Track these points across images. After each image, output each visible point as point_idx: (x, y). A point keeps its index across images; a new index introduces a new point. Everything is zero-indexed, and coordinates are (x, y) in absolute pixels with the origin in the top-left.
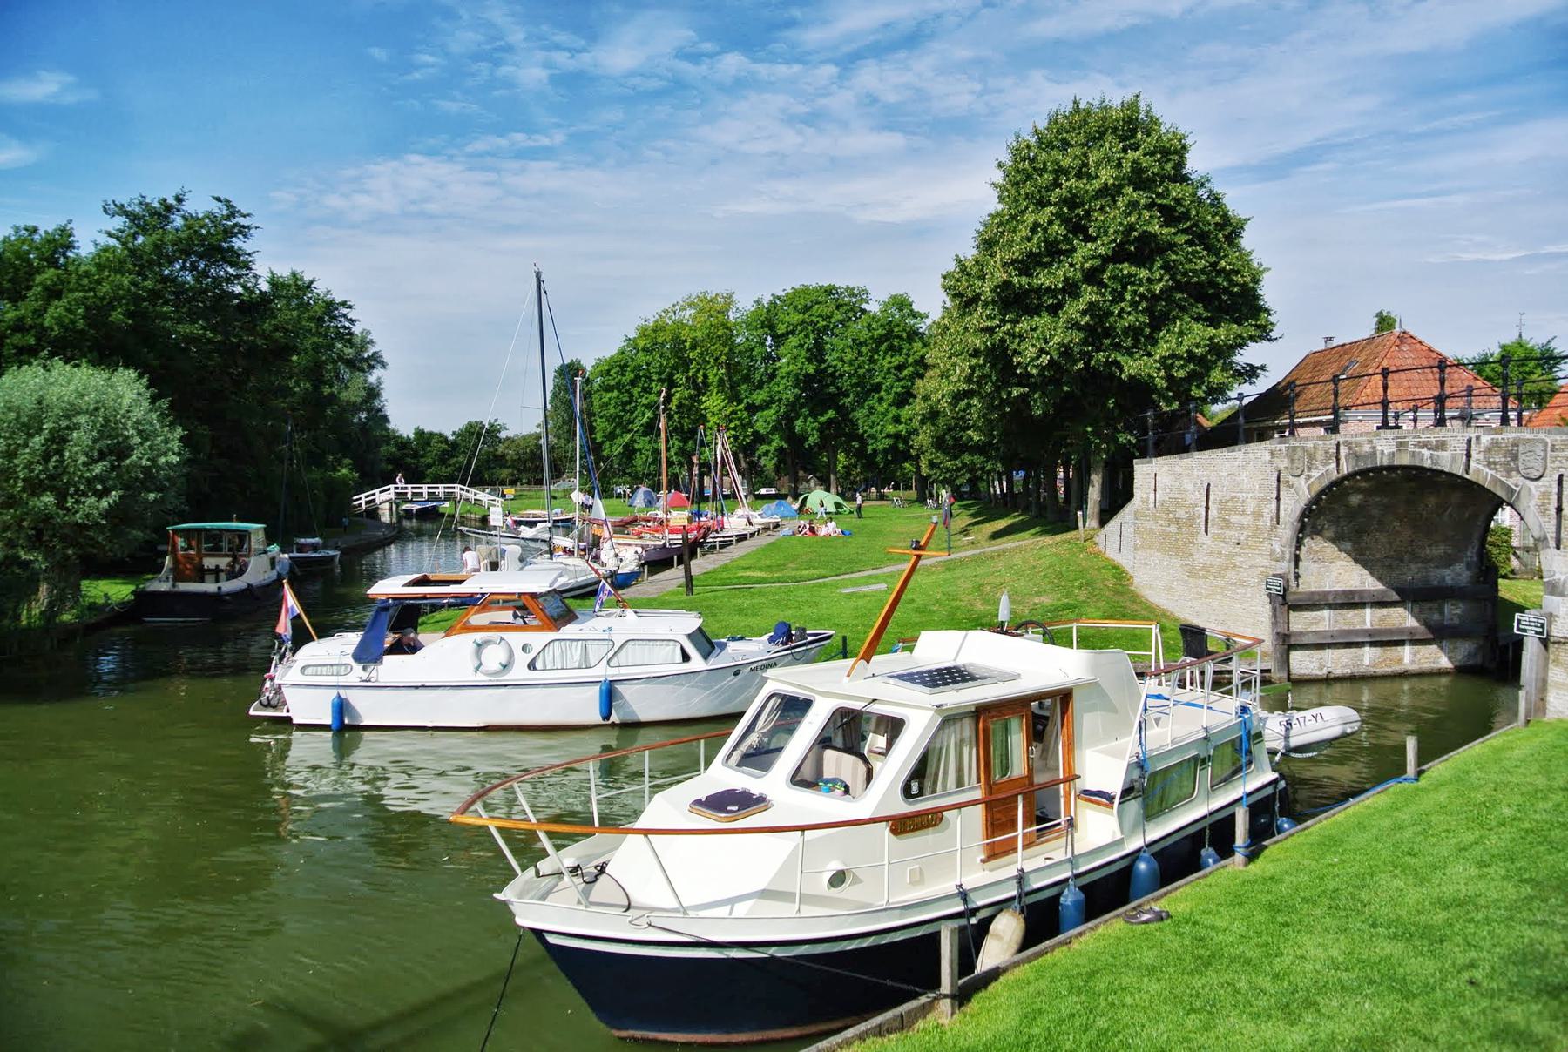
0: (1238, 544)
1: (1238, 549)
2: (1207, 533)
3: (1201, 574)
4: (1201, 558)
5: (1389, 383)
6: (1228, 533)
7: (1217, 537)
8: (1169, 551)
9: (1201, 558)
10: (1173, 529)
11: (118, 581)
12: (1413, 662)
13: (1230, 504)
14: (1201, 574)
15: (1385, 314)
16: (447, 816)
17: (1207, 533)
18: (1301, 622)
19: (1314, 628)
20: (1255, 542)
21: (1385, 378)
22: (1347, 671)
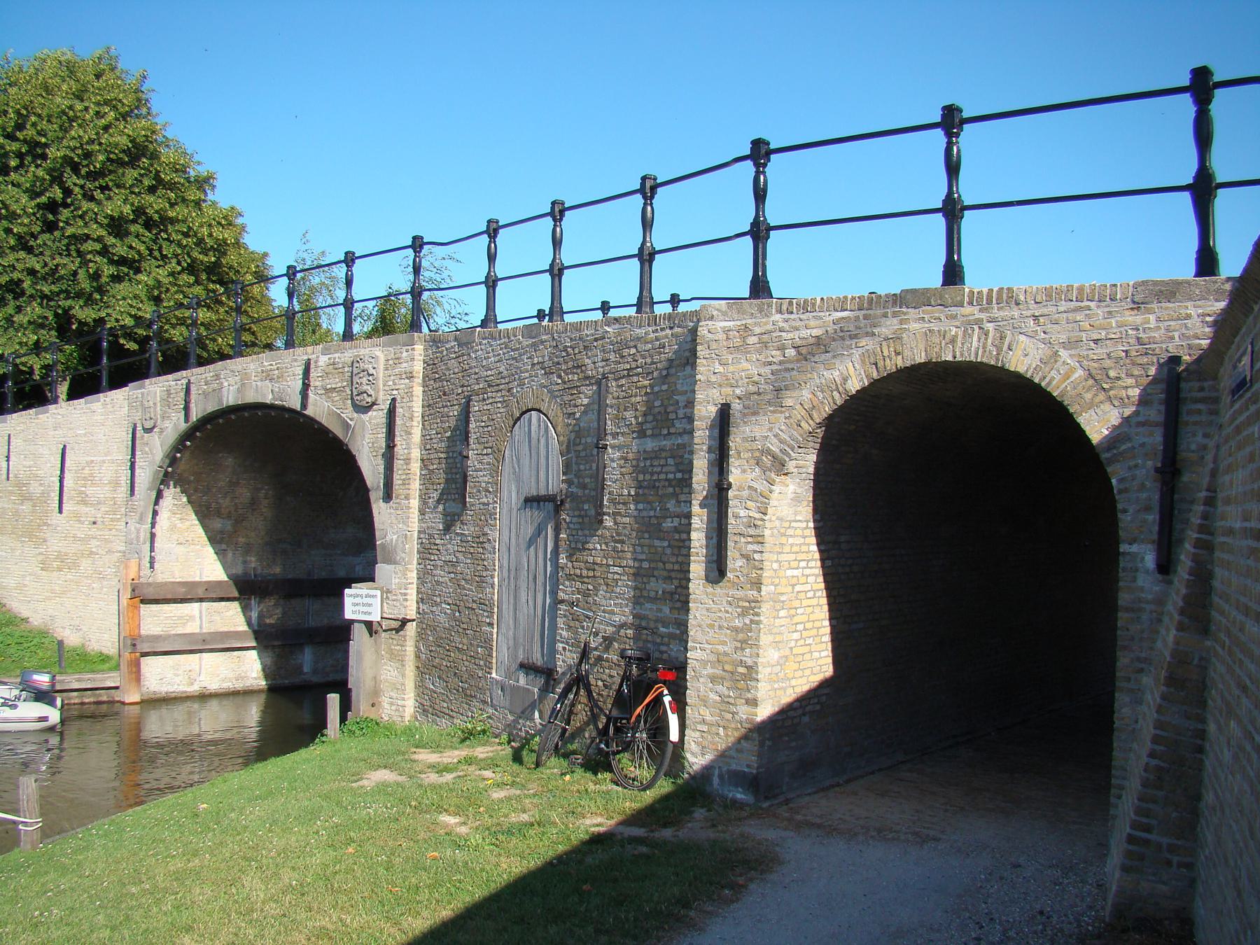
0: (94, 523)
1: (94, 531)
2: (61, 511)
3: (55, 564)
4: (56, 544)
5: (424, 263)
6: (84, 509)
7: (78, 518)
8: (22, 536)
9: (56, 544)
10: (26, 507)
11: (1208, 158)
12: (315, 671)
13: (87, 471)
14: (55, 564)
15: (240, 221)
16: (642, 835)
17: (61, 511)
18: (156, 620)
19: (180, 631)
20: (112, 520)
21: (950, 136)
22: (228, 685)
